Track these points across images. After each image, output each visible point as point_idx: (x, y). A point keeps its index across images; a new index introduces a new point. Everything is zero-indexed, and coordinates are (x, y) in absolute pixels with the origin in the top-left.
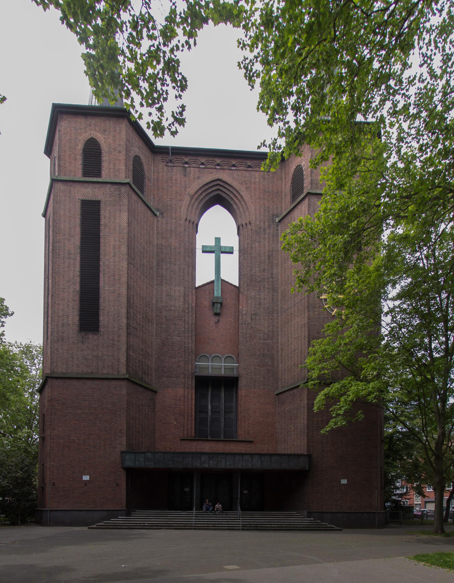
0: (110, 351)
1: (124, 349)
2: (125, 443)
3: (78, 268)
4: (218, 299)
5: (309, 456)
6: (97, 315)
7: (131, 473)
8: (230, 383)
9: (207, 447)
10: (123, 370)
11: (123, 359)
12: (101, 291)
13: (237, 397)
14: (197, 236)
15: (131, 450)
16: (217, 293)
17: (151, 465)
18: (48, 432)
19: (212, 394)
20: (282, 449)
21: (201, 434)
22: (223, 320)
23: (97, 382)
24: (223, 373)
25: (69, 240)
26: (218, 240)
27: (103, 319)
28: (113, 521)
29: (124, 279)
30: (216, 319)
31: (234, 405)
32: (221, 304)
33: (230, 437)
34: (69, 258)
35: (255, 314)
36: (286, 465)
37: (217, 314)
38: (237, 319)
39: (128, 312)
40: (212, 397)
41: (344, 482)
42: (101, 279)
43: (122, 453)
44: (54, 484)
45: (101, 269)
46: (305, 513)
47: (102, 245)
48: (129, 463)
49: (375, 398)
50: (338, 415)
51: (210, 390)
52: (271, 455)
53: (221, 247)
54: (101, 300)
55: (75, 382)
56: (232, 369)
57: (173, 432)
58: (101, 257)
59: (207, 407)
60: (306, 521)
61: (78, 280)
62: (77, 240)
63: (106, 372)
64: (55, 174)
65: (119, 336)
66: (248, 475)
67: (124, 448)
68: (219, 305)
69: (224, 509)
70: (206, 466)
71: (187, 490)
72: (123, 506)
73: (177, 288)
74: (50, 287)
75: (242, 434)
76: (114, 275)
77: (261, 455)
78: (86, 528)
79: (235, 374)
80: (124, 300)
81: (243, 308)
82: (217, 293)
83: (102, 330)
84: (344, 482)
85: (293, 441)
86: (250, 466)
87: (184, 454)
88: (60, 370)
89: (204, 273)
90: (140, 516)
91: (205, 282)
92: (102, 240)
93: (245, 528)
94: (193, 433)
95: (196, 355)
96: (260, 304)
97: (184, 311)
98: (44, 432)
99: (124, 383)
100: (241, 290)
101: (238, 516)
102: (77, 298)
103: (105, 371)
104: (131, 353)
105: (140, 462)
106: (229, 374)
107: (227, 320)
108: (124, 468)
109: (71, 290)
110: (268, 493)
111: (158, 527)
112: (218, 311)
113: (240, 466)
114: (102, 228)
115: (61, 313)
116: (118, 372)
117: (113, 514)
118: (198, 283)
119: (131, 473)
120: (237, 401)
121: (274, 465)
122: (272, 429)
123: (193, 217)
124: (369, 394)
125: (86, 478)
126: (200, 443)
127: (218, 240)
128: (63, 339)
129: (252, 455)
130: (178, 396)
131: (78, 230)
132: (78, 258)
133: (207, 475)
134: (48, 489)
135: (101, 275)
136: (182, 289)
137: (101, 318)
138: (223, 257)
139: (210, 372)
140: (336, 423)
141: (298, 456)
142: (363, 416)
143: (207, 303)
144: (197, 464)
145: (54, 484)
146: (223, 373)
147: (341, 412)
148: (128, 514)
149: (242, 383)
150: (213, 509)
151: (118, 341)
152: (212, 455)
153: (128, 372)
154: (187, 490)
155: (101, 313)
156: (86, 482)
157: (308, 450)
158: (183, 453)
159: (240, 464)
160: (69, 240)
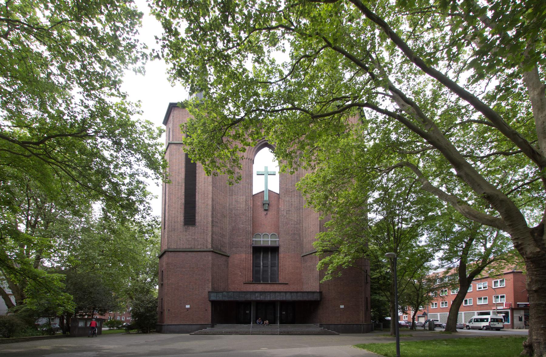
0: (202, 235)
1: (210, 234)
2: (210, 287)
3: (183, 191)
4: (267, 202)
5: (320, 293)
6: (194, 216)
7: (213, 303)
8: (274, 250)
9: (260, 287)
10: (210, 246)
11: (210, 240)
12: (197, 203)
13: (278, 257)
14: (254, 165)
15: (214, 291)
16: (266, 198)
17: (226, 299)
18: (165, 281)
19: (263, 256)
20: (306, 288)
21: (256, 280)
22: (270, 213)
23: (195, 253)
24: (270, 244)
25: (178, 176)
26: (266, 168)
27: (198, 218)
28: (204, 330)
29: (210, 196)
30: (265, 213)
31: (277, 262)
32: (268, 204)
33: (274, 281)
34: (178, 185)
35: (289, 211)
36: (306, 298)
37: (266, 210)
38: (278, 212)
39: (212, 214)
40: (263, 258)
41: (342, 307)
42: (197, 196)
43: (209, 292)
44: (169, 310)
45: (197, 191)
46: (318, 324)
47: (197, 177)
48: (213, 298)
49: (346, 266)
50: (328, 274)
51: (262, 254)
52: (297, 292)
53: (268, 172)
54: (197, 208)
55: (181, 254)
56: (276, 241)
57: (240, 281)
58: (197, 184)
59: (260, 264)
60: (319, 329)
61: (183, 197)
62: (183, 175)
63: (199, 248)
64: (169, 139)
65: (207, 228)
66: (284, 304)
67: (210, 290)
68: (267, 205)
69: (270, 323)
70: (259, 299)
71: (248, 312)
72: (209, 322)
73: (242, 197)
74: (167, 201)
75: (281, 280)
76: (204, 194)
77: (291, 292)
78: (188, 335)
79: (277, 245)
80: (210, 208)
81: (282, 207)
82: (266, 198)
83: (197, 224)
84: (342, 307)
85: (311, 285)
86: (284, 299)
87: (246, 293)
88: (172, 247)
89: (258, 186)
90: (219, 327)
91: (259, 192)
92: (197, 175)
93: (281, 333)
94: (251, 279)
95: (253, 234)
96: (292, 205)
97: (245, 210)
98: (162, 281)
99: (210, 254)
100: (280, 196)
101: (278, 327)
102: (183, 207)
103: (199, 247)
104: (214, 236)
105: (220, 297)
106: (274, 245)
107: (272, 213)
108: (210, 301)
109: (180, 203)
110: (297, 314)
111: (230, 333)
112: (267, 208)
113: (278, 299)
114: (197, 168)
115: (173, 216)
116: (207, 247)
117: (204, 326)
118: (254, 192)
119: (213, 303)
120: (278, 259)
121: (299, 298)
122: (303, 276)
123: (250, 156)
124: (344, 263)
125: (188, 306)
126: (256, 285)
127: (266, 168)
128: (174, 230)
129: (286, 292)
130: (242, 258)
131: (183, 170)
132: (184, 185)
133: (260, 304)
134: (166, 313)
135: (197, 194)
136: (244, 197)
137: (197, 218)
138: (270, 177)
139: (262, 244)
140: (327, 278)
141: (314, 293)
142: (341, 274)
143: (260, 204)
144: (253, 298)
145: (169, 310)
146: (270, 244)
147: (330, 272)
148: (212, 326)
149: (281, 250)
150: (263, 323)
151: (207, 230)
152: (261, 293)
153: (212, 247)
154: (248, 312)
155: (197, 215)
156: (188, 309)
157: (320, 289)
158: (244, 292)
159: (279, 298)
160: (178, 176)
